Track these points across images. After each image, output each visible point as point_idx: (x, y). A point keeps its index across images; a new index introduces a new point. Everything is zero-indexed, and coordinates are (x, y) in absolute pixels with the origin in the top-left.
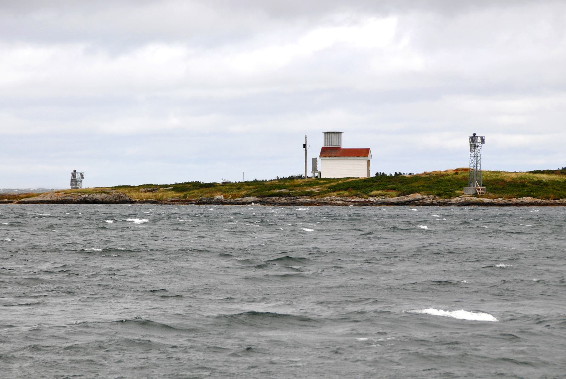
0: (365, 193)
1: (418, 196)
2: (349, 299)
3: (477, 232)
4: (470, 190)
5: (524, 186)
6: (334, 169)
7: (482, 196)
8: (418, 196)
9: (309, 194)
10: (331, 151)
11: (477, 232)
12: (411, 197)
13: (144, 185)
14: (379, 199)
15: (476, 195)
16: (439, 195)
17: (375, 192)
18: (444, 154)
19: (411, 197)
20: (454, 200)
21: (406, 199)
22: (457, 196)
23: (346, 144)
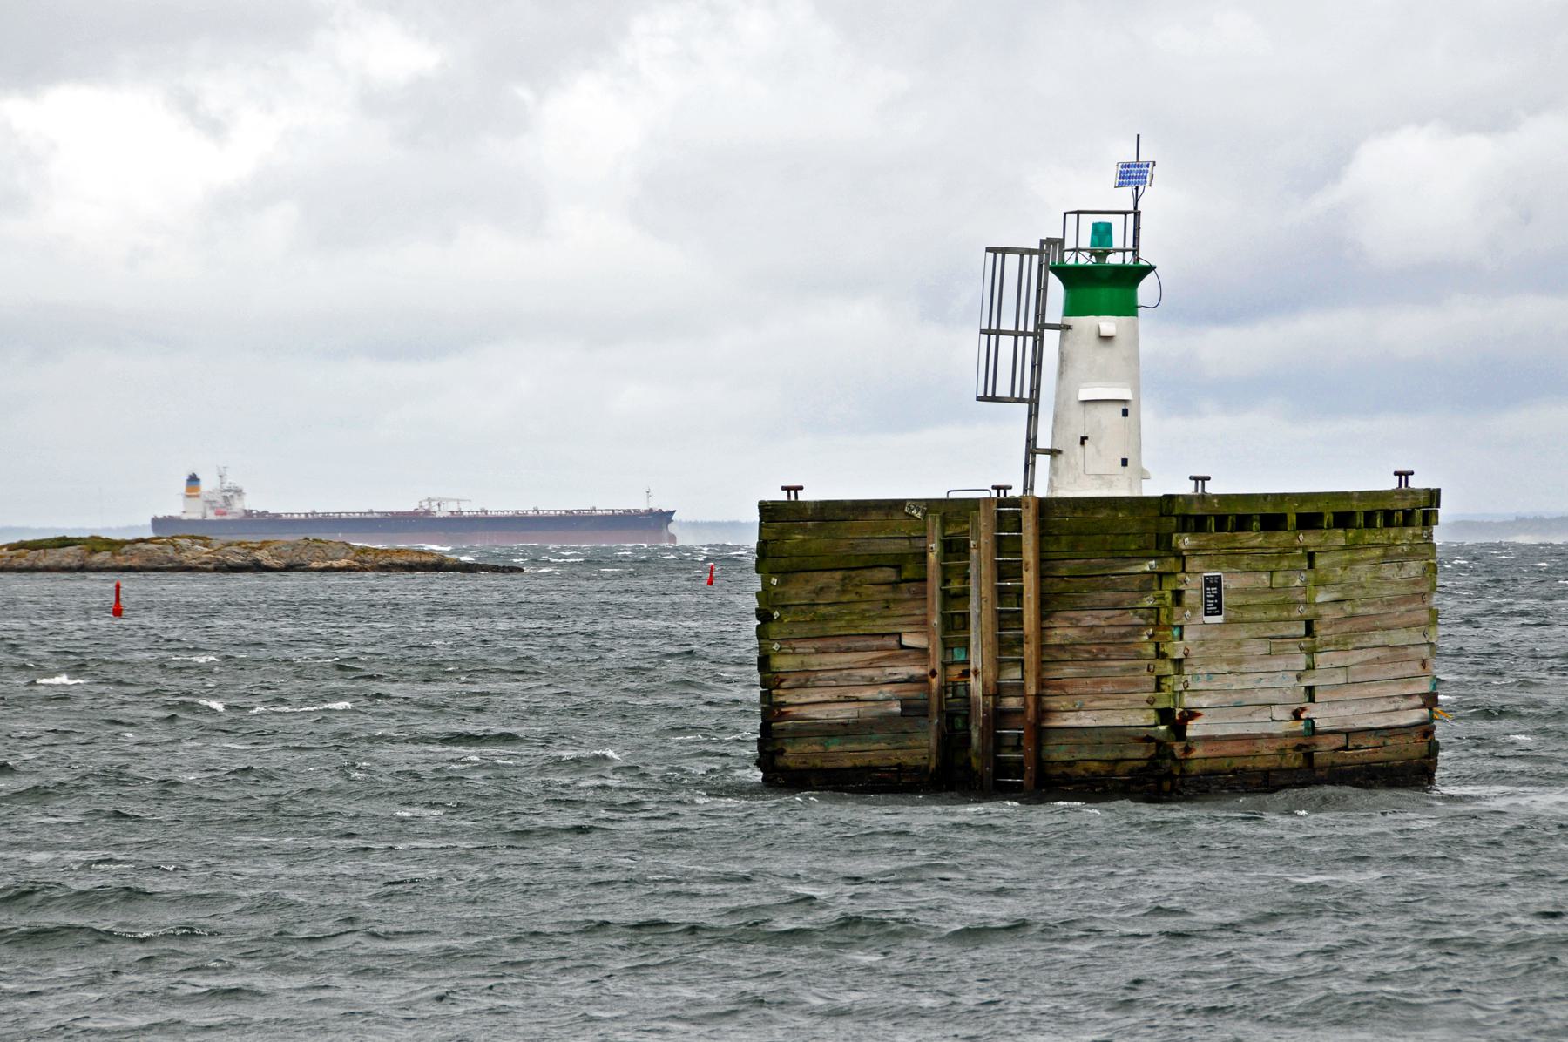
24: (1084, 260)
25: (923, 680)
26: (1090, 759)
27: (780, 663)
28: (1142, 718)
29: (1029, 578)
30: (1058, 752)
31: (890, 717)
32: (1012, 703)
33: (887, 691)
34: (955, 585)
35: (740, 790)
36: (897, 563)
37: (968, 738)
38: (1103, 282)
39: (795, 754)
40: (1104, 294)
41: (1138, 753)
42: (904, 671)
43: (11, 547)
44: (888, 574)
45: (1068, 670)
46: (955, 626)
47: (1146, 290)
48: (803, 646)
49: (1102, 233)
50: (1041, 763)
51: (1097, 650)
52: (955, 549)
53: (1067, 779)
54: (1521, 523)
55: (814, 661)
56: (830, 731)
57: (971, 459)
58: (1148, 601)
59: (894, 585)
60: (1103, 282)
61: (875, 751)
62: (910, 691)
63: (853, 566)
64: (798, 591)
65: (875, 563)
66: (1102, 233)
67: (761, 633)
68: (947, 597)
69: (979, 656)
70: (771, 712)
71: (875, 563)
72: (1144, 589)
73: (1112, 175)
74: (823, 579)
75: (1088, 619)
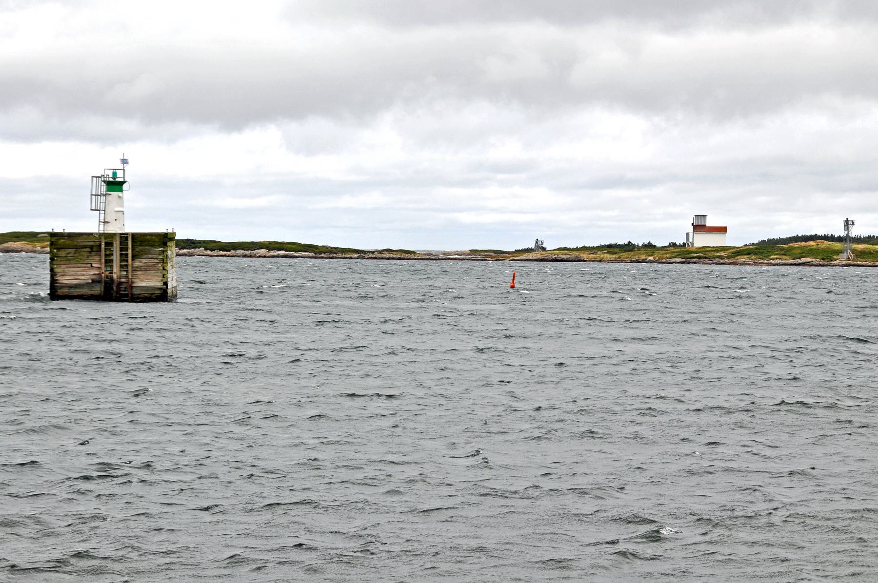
0: (767, 257)
1: (808, 260)
2: (633, 535)
3: (774, 336)
4: (845, 256)
5: (871, 253)
6: (701, 241)
7: (853, 260)
8: (808, 260)
9: (720, 257)
10: (699, 227)
11: (774, 336)
12: (803, 260)
13: (605, 246)
14: (778, 261)
15: (849, 259)
16: (823, 259)
17: (772, 257)
18: (672, 229)
19: (803, 260)
20: (835, 262)
21: (799, 262)
22: (836, 260)
23: (710, 223)
24: (111, 180)
25: (99, 274)
26: (146, 293)
27: (56, 270)
28: (159, 284)
29: (130, 252)
30: (136, 292)
31: (88, 283)
32: (123, 280)
33: (88, 277)
34: (108, 253)
35: (35, 299)
36: (91, 247)
37: (112, 289)
38: (115, 185)
39: (60, 292)
40: (116, 187)
41: (158, 292)
42: (92, 272)
43: (560, 249)
44: (89, 250)
45: (139, 273)
46: (109, 262)
47: (125, 186)
48: (63, 266)
49: (115, 174)
50: (132, 294)
51: (146, 269)
52: (109, 244)
53: (138, 298)
54: (746, 246)
55: (66, 270)
56: (71, 287)
57: (89, 225)
58: (161, 257)
59: (90, 252)
60: (115, 185)
61: (85, 291)
62: (94, 277)
63: (77, 248)
64: (62, 253)
65: (85, 247)
66: (115, 174)
67: (51, 263)
68: (106, 255)
69: (116, 269)
70: (53, 282)
71: (85, 247)
72: (159, 255)
73: (129, 161)
74: (70, 250)
75: (144, 261)
